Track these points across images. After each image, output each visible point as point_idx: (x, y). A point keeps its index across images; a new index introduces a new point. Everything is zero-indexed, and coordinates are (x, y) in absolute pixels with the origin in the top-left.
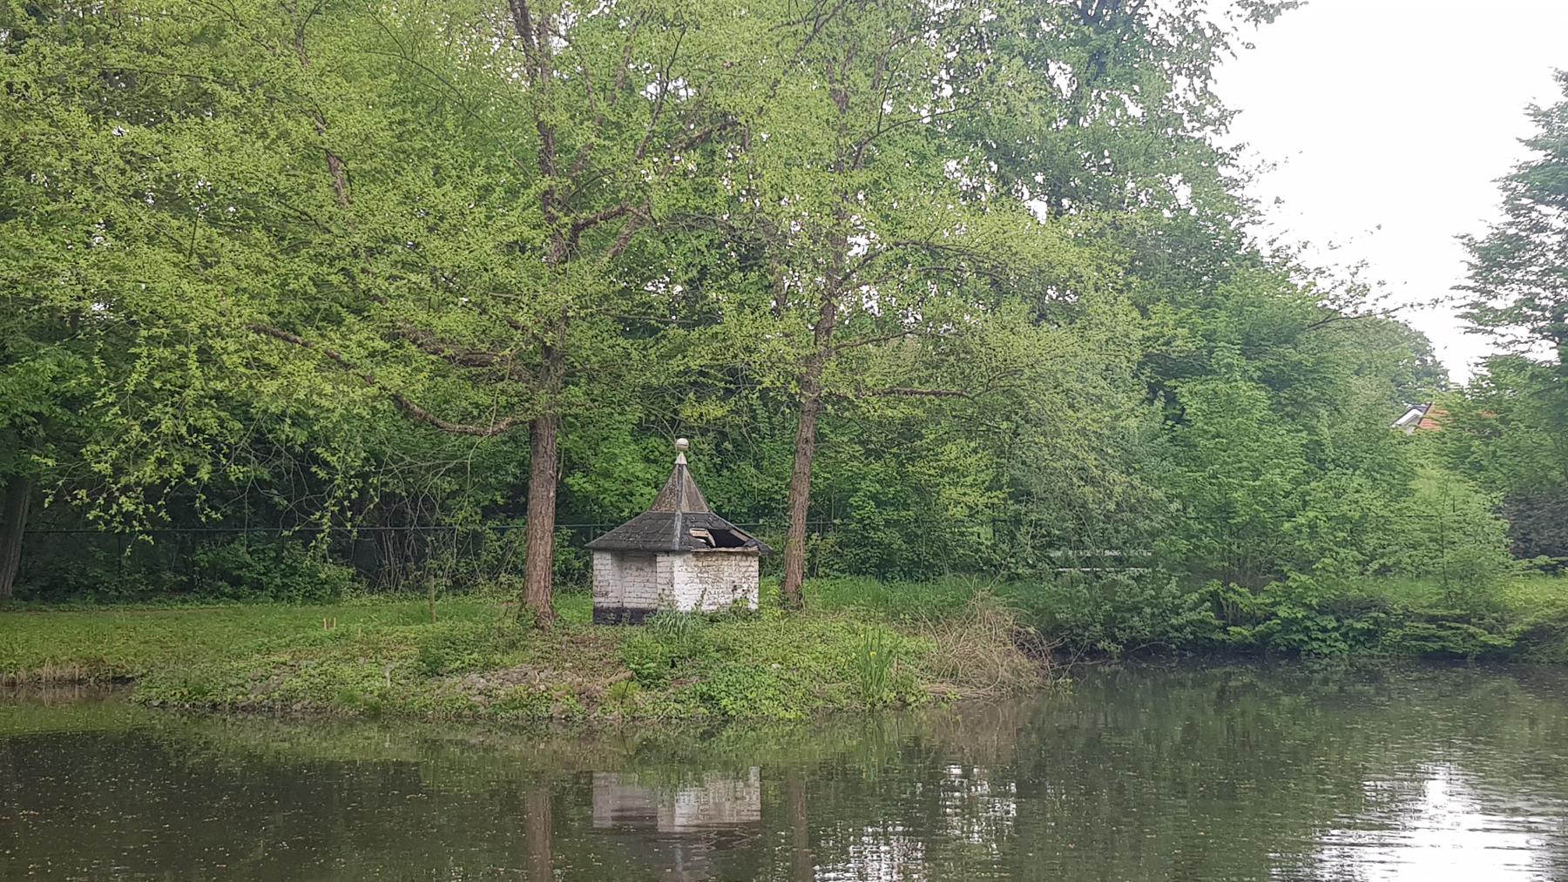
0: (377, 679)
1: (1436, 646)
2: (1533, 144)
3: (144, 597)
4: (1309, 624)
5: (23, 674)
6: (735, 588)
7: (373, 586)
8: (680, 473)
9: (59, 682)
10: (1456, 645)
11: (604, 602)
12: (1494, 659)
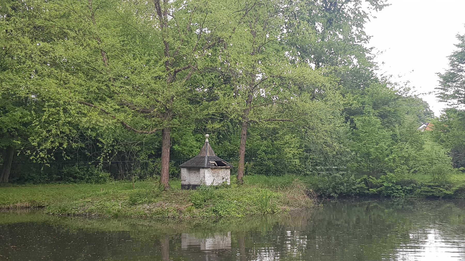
0: (117, 206)
1: (431, 194)
2: (458, 46)
3: (48, 182)
4: (393, 188)
5: (11, 205)
6: (223, 178)
7: (115, 178)
8: (207, 144)
9: (22, 208)
10: (436, 194)
11: (184, 183)
12: (447, 198)
